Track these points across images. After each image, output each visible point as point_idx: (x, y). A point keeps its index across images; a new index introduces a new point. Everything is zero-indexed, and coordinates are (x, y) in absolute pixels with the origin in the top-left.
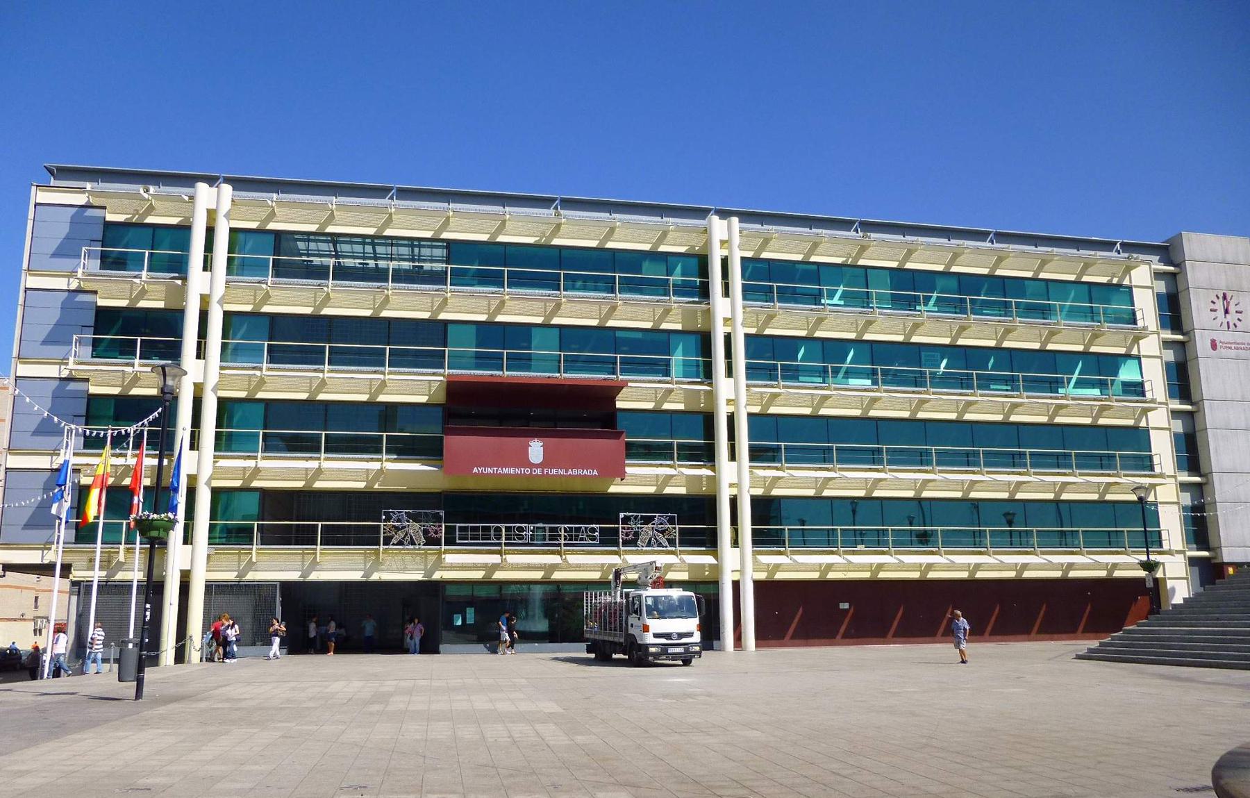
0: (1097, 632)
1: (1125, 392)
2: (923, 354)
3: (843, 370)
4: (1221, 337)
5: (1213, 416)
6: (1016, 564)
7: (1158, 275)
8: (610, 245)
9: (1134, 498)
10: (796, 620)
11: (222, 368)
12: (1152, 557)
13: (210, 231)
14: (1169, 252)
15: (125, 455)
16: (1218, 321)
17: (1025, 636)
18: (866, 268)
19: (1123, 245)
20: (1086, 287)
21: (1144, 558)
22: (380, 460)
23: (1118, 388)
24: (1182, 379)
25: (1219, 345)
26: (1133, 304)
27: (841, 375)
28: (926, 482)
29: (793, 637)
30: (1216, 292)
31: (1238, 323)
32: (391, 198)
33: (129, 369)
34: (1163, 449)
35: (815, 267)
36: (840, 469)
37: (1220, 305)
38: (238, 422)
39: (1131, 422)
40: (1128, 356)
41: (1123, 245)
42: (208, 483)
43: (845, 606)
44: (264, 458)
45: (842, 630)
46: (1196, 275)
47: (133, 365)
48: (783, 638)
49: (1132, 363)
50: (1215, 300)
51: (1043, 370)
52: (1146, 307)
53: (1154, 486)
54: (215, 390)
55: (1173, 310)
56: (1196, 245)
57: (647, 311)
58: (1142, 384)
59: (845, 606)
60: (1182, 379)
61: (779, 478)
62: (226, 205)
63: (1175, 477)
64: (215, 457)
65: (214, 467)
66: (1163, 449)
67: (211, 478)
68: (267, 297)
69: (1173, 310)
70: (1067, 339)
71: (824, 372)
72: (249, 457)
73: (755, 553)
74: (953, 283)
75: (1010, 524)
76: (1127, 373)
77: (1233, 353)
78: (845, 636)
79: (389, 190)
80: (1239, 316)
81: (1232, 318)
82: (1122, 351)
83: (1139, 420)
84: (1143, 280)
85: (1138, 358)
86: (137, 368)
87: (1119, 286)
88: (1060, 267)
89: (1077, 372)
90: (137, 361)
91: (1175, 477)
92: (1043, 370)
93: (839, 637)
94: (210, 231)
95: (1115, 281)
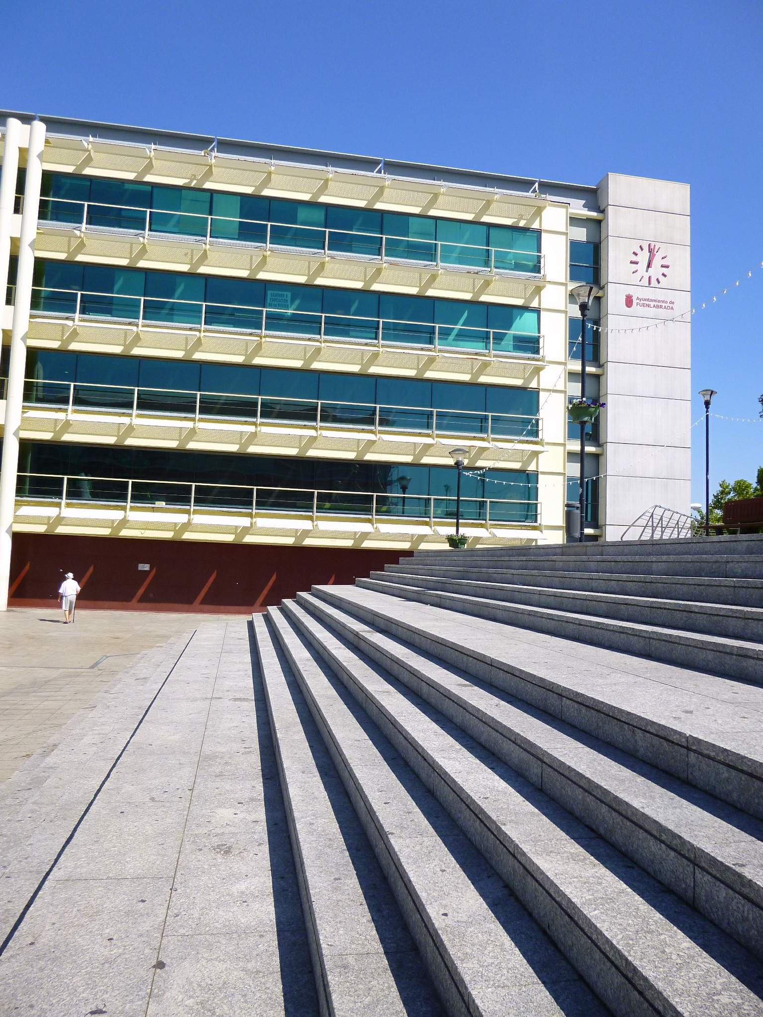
0: (95, 599)
1: (517, 348)
2: (269, 293)
3: (455, 333)
4: (636, 293)
5: (616, 380)
6: (237, 527)
7: (574, 221)
8: (266, 192)
9: (451, 462)
10: (209, 584)
11: (32, 316)
12: (463, 531)
13: (22, 174)
14: (595, 197)
15: (66, 410)
16: (638, 276)
17: (186, 606)
18: (212, 192)
19: (542, 185)
20: (485, 228)
21: (452, 531)
22: (193, 420)
23: (508, 342)
24: (588, 340)
25: (635, 301)
26: (539, 250)
27: (451, 337)
28: (428, 446)
29: (203, 602)
30: (641, 243)
31: (661, 278)
32: (534, 191)
33: (70, 323)
34: (553, 416)
35: (149, 188)
36: (494, 440)
37: (644, 257)
38: (514, 408)
39: (519, 382)
40: (525, 308)
41: (542, 185)
42: (16, 434)
43: (146, 567)
44: (138, 416)
45: (141, 592)
46: (617, 222)
47: (73, 320)
48: (130, 601)
49: (530, 317)
50: (638, 251)
51: (417, 317)
52: (555, 257)
53: (536, 454)
54: (24, 339)
55: (588, 262)
56: (622, 188)
57: (467, 281)
58: (536, 340)
59: (146, 567)
60: (588, 340)
61: (431, 445)
62: (38, 146)
63: (564, 445)
64: (24, 407)
65: (23, 420)
66: (553, 416)
67: (19, 429)
68: (143, 251)
69: (588, 262)
70: (450, 283)
71: (485, 337)
72: (60, 410)
73: (18, 504)
74: (320, 215)
75: (404, 489)
76: (523, 326)
77: (651, 312)
78: (142, 600)
79: (376, 163)
80: (665, 270)
81: (656, 271)
82: (519, 302)
83: (530, 379)
84: (557, 224)
85: (538, 311)
86: (77, 322)
87: (525, 230)
88: (453, 203)
89: (462, 321)
90: (77, 315)
91: (564, 445)
92: (417, 317)
93: (134, 601)
94: (22, 174)
95: (522, 224)
